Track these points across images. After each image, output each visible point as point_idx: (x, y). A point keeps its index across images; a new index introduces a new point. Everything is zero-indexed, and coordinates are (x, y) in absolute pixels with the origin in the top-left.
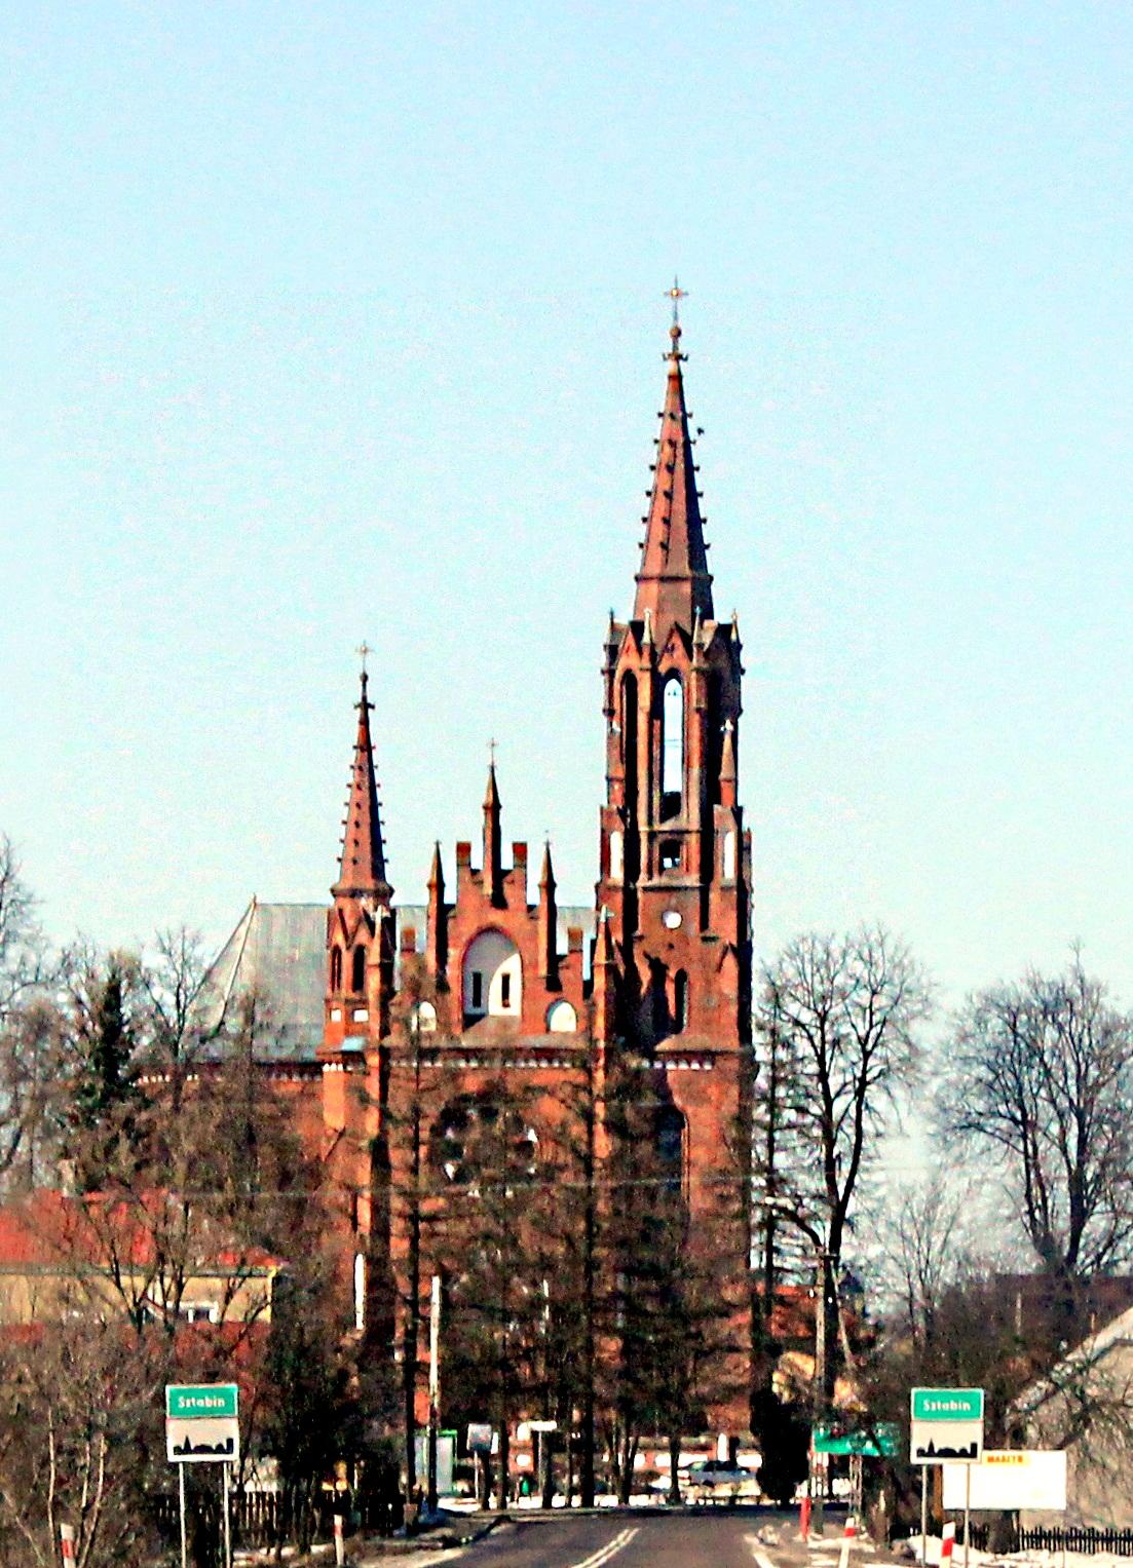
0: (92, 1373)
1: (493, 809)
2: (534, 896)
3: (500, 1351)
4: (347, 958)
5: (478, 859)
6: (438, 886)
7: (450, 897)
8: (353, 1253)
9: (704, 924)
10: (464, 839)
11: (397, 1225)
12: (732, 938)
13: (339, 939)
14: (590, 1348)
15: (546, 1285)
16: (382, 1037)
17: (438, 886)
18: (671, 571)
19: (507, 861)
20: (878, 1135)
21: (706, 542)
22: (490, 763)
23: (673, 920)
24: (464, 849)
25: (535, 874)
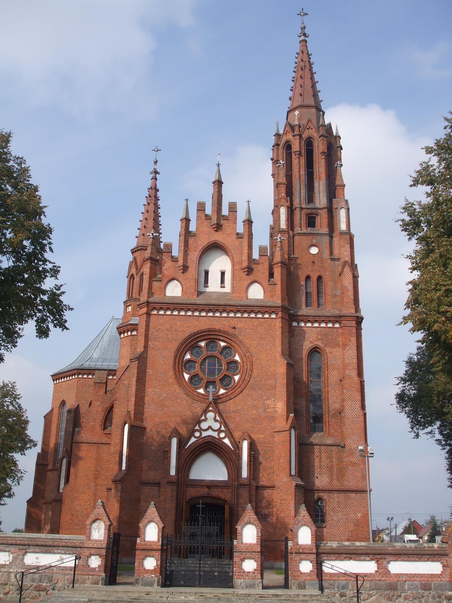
0: (275, 483)
1: (219, 183)
2: (240, 228)
3: (416, 358)
4: (137, 280)
5: (209, 210)
6: (187, 220)
7: (193, 227)
8: (122, 422)
9: (331, 253)
10: (202, 200)
11: (236, 496)
12: (348, 259)
13: (134, 271)
14: (8, 432)
15: (327, 273)
16: (148, 297)
17: (187, 220)
18: (307, 103)
19: (225, 211)
20: (39, 589)
21: (320, 99)
22: (214, 178)
23: (314, 250)
24: (201, 207)
25: (241, 216)
